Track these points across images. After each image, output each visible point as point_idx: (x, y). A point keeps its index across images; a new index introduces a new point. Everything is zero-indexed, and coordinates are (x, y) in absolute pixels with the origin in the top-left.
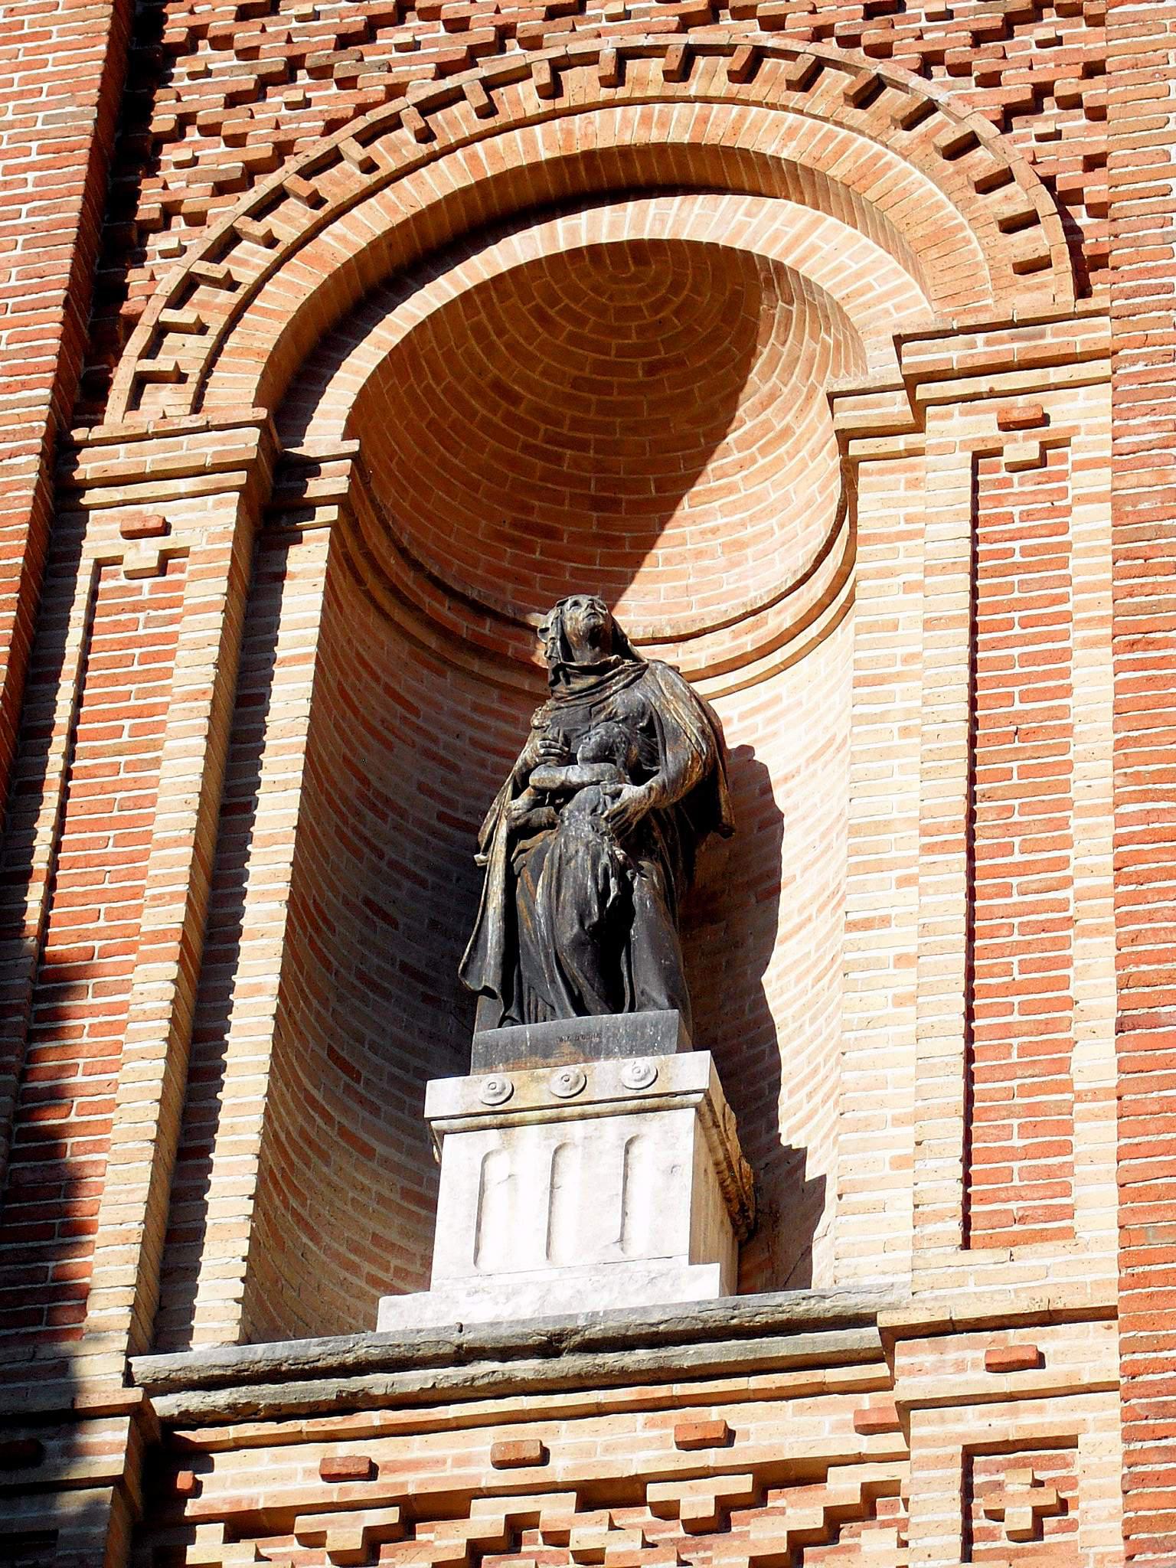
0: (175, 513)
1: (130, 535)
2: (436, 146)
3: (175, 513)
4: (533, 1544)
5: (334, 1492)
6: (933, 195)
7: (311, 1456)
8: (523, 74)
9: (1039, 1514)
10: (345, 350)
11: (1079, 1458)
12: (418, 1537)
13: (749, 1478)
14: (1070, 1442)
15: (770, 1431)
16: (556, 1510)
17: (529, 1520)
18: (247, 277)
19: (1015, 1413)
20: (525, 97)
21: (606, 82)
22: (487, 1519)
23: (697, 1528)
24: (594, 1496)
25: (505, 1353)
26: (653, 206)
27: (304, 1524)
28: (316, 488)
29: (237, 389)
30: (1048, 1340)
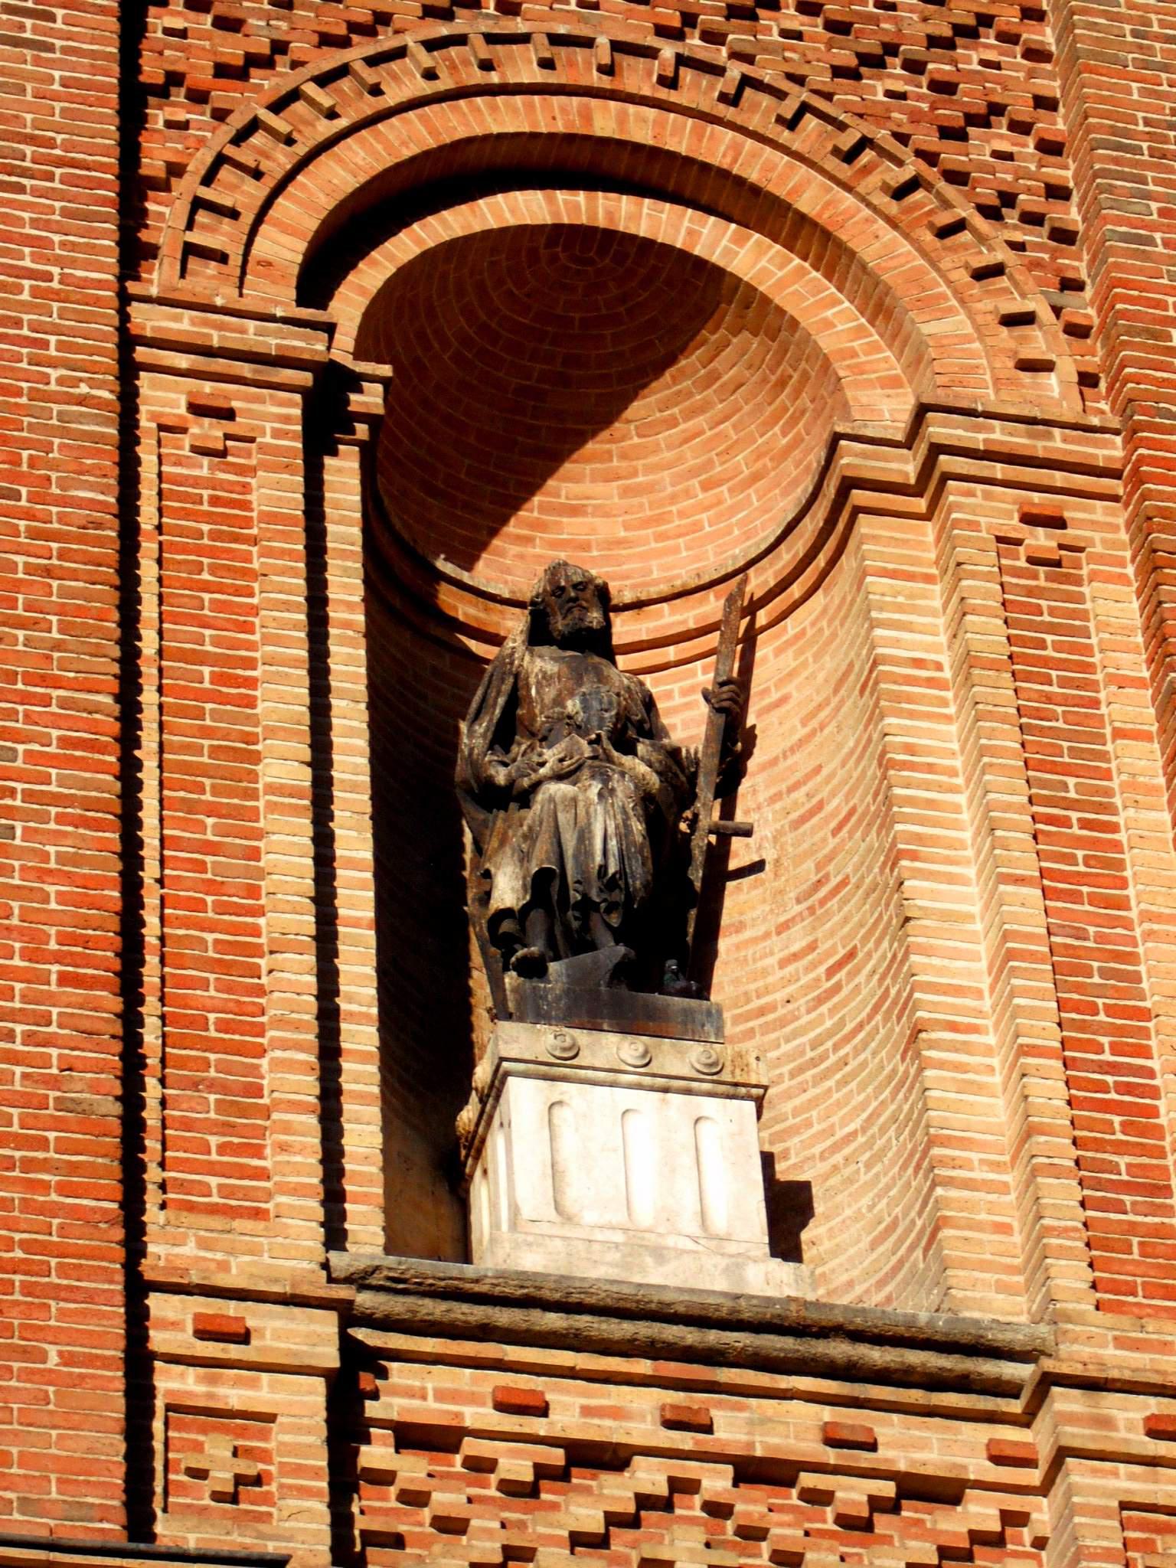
0: (1074, 510)
1: (1030, 519)
2: (495, 78)
3: (1074, 510)
4: (691, 1508)
5: (832, 1456)
6: (946, 298)
7: (981, 1434)
8: (718, 71)
9: (240, 1480)
10: (376, 242)
11: (279, 1437)
12: (574, 1481)
13: (561, 1452)
14: (271, 1418)
15: (913, 1444)
16: (717, 1482)
17: (691, 1486)
18: (393, 96)
19: (254, 1385)
20: (696, 91)
21: (723, 98)
22: (980, 1512)
23: (512, 1489)
24: (751, 1471)
25: (857, 1336)
26: (625, 203)
27: (471, 1446)
28: (357, 401)
29: (284, 246)
30: (253, 1315)
